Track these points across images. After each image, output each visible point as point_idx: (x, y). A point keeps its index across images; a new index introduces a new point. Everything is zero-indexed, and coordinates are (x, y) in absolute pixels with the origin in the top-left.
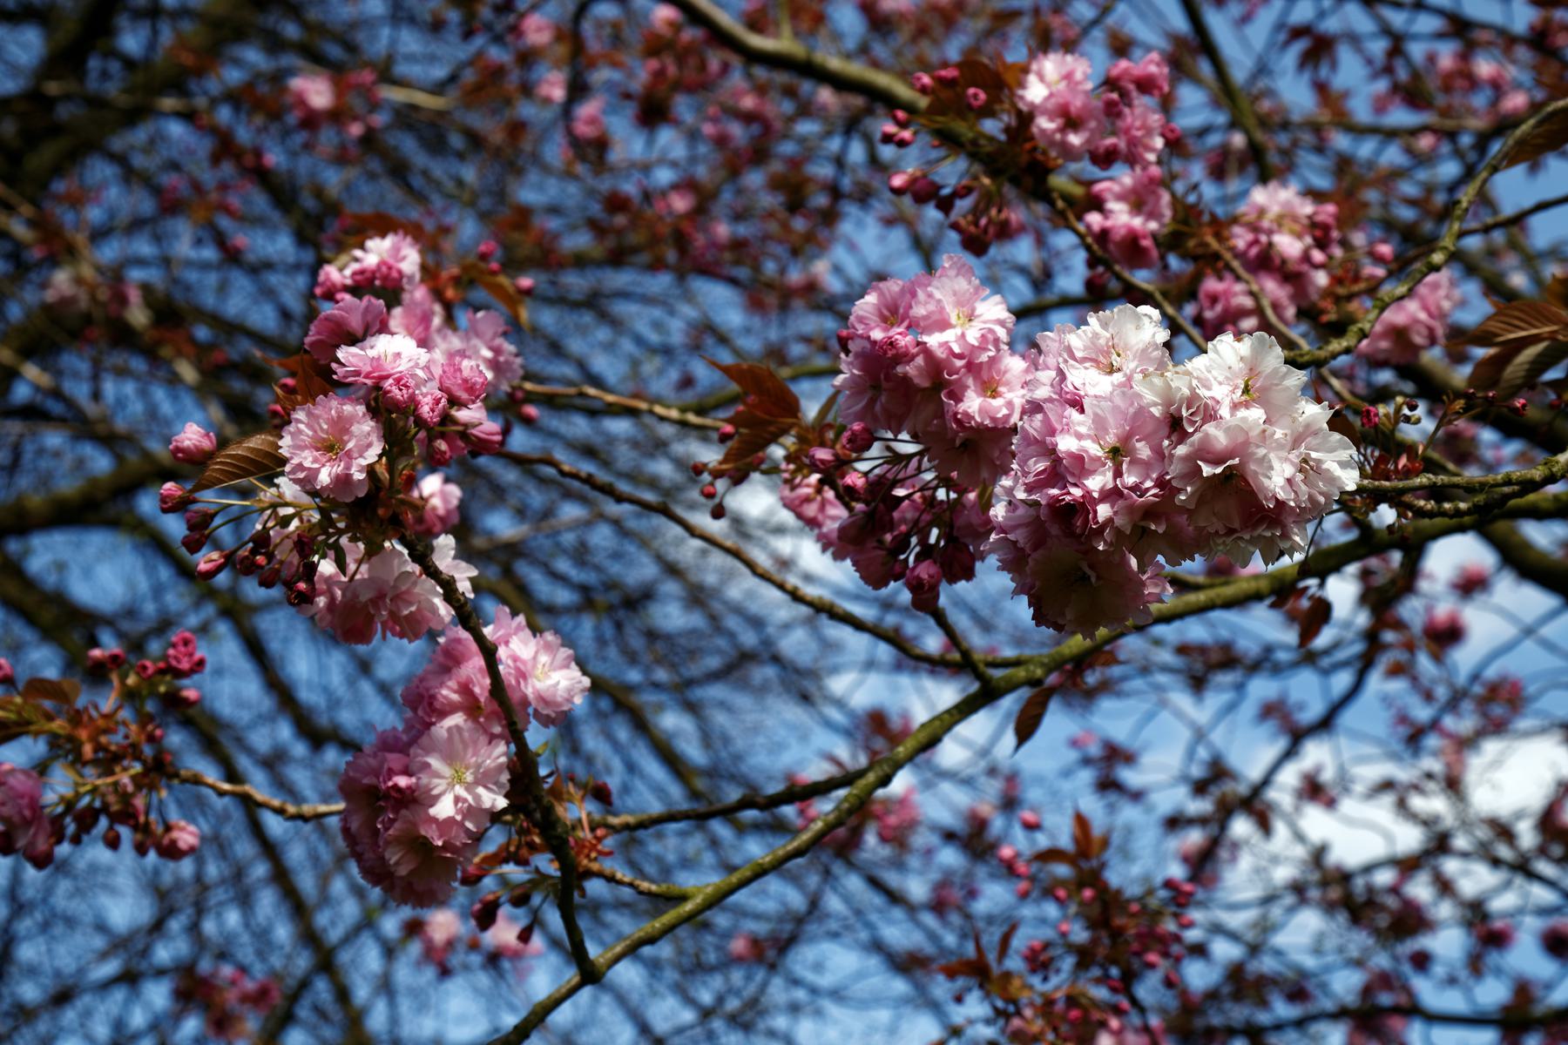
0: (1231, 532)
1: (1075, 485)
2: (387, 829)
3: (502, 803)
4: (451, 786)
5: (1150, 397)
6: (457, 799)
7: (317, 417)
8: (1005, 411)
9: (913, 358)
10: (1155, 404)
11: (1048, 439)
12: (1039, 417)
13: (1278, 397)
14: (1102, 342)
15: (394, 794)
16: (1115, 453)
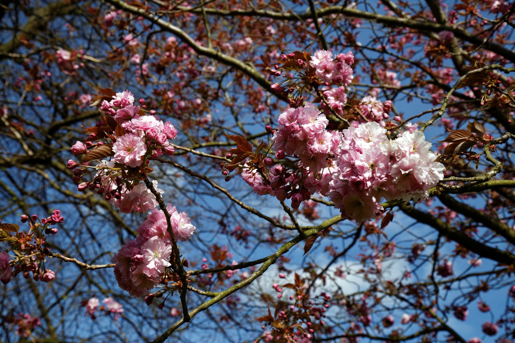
0: (408, 191)
1: (361, 175)
2: (132, 271)
3: (169, 265)
4: (154, 258)
5: (384, 150)
6: (156, 263)
7: (125, 141)
8: (326, 148)
9: (299, 131)
10: (385, 152)
11: (352, 161)
12: (347, 154)
13: (422, 151)
14: (366, 132)
15: (136, 260)
16: (372, 166)
